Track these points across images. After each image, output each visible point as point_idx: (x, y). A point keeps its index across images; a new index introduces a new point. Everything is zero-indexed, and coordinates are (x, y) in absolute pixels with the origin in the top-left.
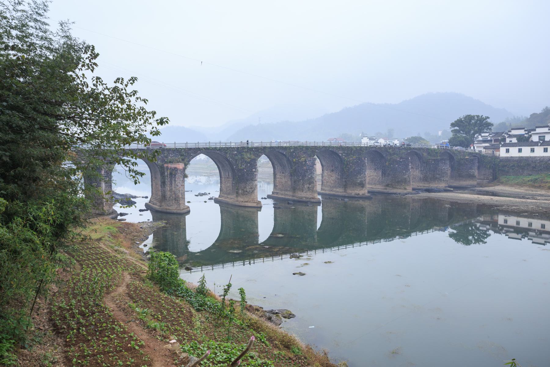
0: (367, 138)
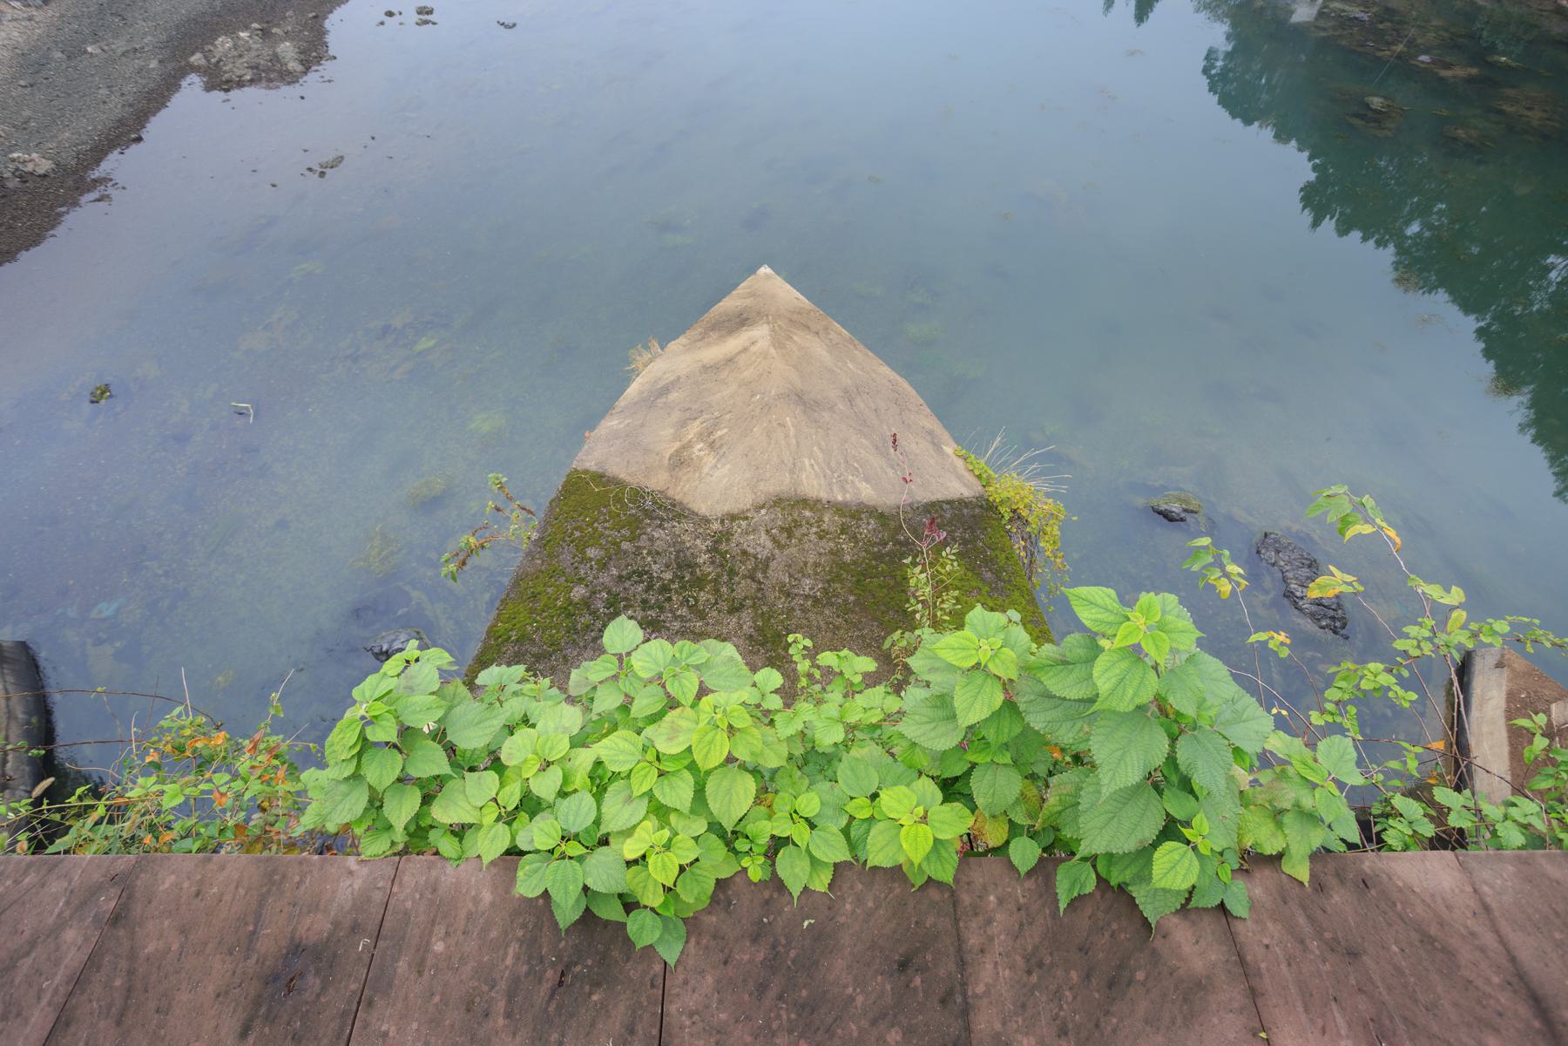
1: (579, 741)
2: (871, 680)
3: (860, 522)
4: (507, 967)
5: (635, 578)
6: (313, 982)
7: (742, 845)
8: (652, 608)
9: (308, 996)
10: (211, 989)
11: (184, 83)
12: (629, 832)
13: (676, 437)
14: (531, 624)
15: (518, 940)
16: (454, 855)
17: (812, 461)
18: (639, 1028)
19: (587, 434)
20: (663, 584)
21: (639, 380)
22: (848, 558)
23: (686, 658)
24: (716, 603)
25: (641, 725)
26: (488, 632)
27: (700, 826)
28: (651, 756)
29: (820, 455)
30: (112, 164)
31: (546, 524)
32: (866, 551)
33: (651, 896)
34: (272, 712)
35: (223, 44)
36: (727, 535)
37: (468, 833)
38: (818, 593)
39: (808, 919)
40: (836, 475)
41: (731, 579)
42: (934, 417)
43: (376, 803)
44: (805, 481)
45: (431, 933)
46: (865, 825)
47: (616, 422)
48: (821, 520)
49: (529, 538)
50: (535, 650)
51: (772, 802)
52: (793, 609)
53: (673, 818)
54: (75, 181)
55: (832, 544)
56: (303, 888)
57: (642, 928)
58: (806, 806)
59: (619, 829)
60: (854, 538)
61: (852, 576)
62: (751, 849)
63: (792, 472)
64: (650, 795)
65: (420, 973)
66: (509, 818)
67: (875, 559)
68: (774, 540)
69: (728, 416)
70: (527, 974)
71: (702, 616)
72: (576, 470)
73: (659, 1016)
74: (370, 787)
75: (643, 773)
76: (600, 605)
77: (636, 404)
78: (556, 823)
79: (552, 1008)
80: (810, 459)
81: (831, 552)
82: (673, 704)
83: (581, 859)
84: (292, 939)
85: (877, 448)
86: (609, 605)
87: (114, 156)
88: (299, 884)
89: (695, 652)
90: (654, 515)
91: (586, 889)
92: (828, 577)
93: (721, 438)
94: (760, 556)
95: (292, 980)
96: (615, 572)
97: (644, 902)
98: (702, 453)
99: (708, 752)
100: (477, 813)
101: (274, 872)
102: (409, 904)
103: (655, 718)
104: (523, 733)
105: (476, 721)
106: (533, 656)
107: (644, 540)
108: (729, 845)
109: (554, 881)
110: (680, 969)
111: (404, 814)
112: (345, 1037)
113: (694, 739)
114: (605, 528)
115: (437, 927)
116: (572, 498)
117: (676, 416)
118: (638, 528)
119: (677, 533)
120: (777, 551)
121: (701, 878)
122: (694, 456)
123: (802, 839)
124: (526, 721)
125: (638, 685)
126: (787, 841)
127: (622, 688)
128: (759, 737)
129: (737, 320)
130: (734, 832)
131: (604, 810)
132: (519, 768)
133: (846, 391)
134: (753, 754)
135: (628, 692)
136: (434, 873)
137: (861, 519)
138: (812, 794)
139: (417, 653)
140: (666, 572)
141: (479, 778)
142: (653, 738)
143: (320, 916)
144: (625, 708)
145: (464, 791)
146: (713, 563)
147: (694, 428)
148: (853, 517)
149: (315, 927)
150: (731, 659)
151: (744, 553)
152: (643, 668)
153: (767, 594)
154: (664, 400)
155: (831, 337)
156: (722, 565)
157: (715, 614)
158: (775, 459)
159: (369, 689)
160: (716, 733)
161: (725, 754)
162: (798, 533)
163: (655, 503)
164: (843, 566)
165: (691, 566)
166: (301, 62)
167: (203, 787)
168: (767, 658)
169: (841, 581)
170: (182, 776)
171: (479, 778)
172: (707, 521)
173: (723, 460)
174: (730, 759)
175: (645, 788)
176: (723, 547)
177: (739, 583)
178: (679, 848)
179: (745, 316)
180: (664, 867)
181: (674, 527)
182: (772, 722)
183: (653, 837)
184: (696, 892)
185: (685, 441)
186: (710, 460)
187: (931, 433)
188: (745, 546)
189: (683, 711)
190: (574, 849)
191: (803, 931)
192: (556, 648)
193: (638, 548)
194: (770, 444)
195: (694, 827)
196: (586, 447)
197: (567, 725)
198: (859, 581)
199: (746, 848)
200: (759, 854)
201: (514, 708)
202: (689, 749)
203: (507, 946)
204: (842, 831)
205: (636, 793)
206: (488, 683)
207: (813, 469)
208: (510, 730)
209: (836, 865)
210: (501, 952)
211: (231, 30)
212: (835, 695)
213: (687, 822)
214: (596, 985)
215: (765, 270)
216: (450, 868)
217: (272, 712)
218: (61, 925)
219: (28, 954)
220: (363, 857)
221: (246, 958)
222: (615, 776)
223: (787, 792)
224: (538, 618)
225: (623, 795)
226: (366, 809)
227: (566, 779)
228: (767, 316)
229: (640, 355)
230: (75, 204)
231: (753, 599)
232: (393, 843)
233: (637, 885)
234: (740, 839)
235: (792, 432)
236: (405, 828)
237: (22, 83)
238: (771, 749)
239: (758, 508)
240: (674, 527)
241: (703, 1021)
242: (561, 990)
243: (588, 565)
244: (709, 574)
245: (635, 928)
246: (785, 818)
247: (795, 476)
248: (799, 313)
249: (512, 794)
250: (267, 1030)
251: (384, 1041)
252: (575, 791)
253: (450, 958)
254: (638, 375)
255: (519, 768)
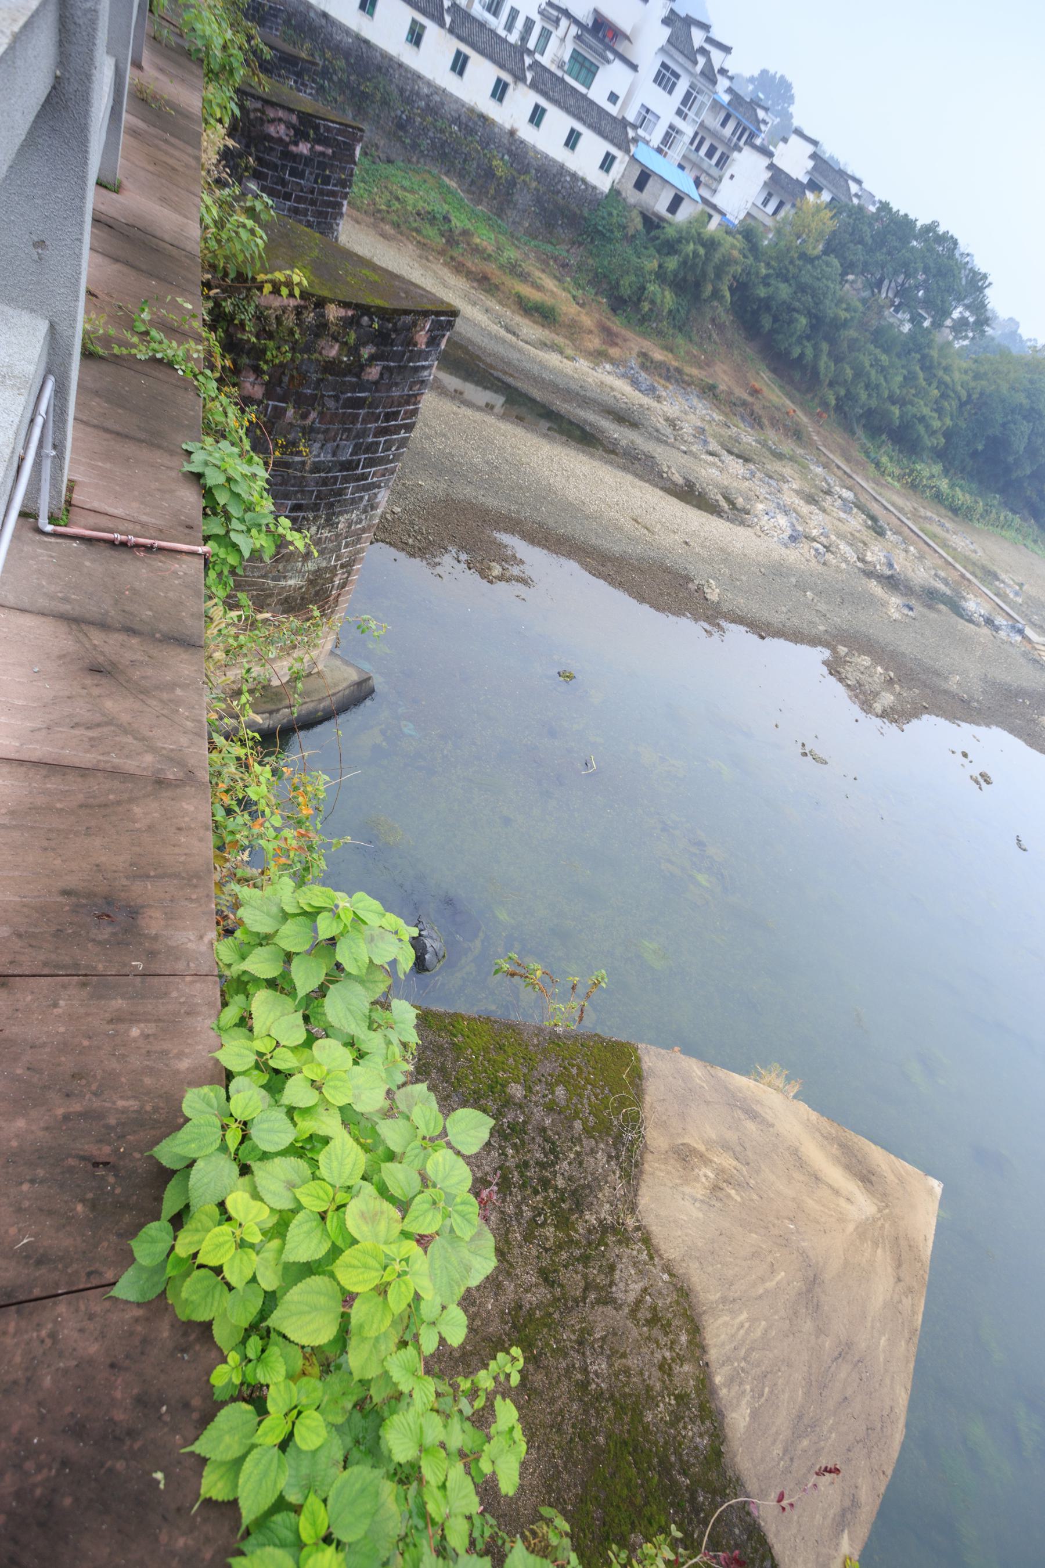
0: (810, 149)
1: (349, 1116)
2: (487, 1490)
3: (698, 1422)
4: (114, 1103)
5: (547, 1146)
6: (105, 932)
7: (254, 1343)
8: (522, 1175)
9: (94, 932)
10: (103, 859)
11: (819, 648)
12: (256, 1196)
13: (708, 1142)
14: (473, 1052)
15: (142, 1107)
16: (222, 1024)
17: (747, 1325)
18: (43, 1270)
19: (676, 1049)
20: (549, 1181)
21: (751, 1083)
22: (649, 1417)
23: (457, 1211)
24: (546, 1250)
25: (375, 1178)
26: (455, 1014)
27: (269, 1282)
28: (342, 1196)
29: (759, 1333)
30: (736, 632)
31: (575, 1037)
32: (666, 1443)
33: (187, 1241)
34: (334, 841)
35: (866, 661)
36: (625, 1240)
37: (245, 1031)
38: (594, 1386)
39: (166, 1477)
40: (743, 1364)
41: (578, 1260)
42: (878, 1501)
43: (264, 940)
44: (720, 1321)
45: (148, 1021)
46: (289, 1536)
47: (699, 1074)
48: (681, 1359)
49: (555, 1025)
50: (449, 1064)
51: (310, 1375)
52: (566, 1355)
53: (275, 1243)
54: (712, 615)
55: (658, 1386)
56: (186, 903)
57: (153, 1241)
58: (308, 1428)
59: (258, 1184)
60: (676, 1418)
61: (629, 1431)
62: (250, 1361)
63: (724, 1300)
64: (298, 1208)
65: (111, 1021)
66: (261, 1064)
67: (661, 1462)
68: (639, 1302)
69: (755, 1197)
70: (108, 1127)
71: (528, 1237)
72: (637, 1049)
73: (54, 1292)
74: (277, 931)
75: (322, 1194)
76: (510, 1117)
77: (726, 1088)
78: (259, 1110)
79: (71, 1162)
80: (748, 1319)
81: (649, 1389)
82: (403, 1207)
83: (223, 1148)
84: (143, 907)
85: (800, 1417)
86: (512, 1127)
87: (742, 629)
88: (190, 900)
89: (468, 1221)
90: (620, 1146)
91: (191, 1165)
92: (617, 1395)
93: (729, 1196)
94: (614, 1289)
95: (108, 916)
96: (548, 1122)
97: (182, 1235)
98: (703, 1179)
99: (354, 1267)
100: (264, 1032)
101: (199, 878)
102: (175, 994)
103: (383, 1192)
104: (347, 1055)
105: (352, 1008)
106: (443, 1064)
107: (588, 1143)
108: (252, 1329)
109: (198, 1126)
110: (107, 1304)
111: (256, 966)
112: (57, 972)
113: (365, 1244)
114: (589, 1098)
115: (153, 1025)
116: (608, 1055)
117: (732, 1136)
118: (600, 1132)
119: (609, 1179)
120: (627, 1310)
121: (209, 1300)
122: (697, 1170)
123: (265, 1434)
124: (360, 1056)
125: (417, 1164)
126: (262, 1411)
127: (409, 1149)
128: (383, 1330)
129: (865, 1172)
130: (268, 1330)
131: (277, 1160)
132: (312, 1060)
133: (849, 1345)
134: (361, 1326)
135: (407, 1155)
136: (204, 1009)
137: (703, 1423)
138: (324, 1432)
139: (406, 938)
140: (564, 1179)
141: (298, 1026)
142: (361, 1195)
143: (163, 922)
144: (391, 1156)
145: (283, 1015)
146: (589, 1231)
147: (726, 1161)
148: (702, 1407)
149: (153, 923)
150: (468, 1269)
151: (612, 1268)
152: (436, 1164)
153: (574, 1313)
154: (742, 1117)
155: (904, 1300)
156: (590, 1244)
157: (534, 1252)
158: (731, 1272)
159: (367, 905)
160: (377, 1270)
161: (354, 1289)
162: (656, 1332)
163: (632, 1142)
164: (638, 1415)
165: (579, 1207)
166: (884, 711)
167: (267, 811)
168: (500, 1338)
169: (618, 1417)
170: (274, 796)
171: (298, 1026)
172: (633, 1209)
173: (705, 1207)
174: (349, 1299)
175: (304, 1201)
176: (611, 1239)
177: (577, 1273)
178: (241, 1260)
179: (873, 1178)
180: (219, 1246)
181: (614, 1173)
182: (403, 1344)
183: (252, 1223)
184: (194, 1297)
185: (709, 1155)
186: (699, 1191)
187: (855, 1503)
188: (619, 1266)
189: (397, 1221)
190: (233, 1138)
191: (150, 1473)
192: (456, 1084)
193: (580, 1140)
194: (745, 1259)
195: (268, 1273)
196: (663, 1052)
197: (363, 1097)
198: (625, 1443)
199: (251, 1354)
200: (244, 1375)
201: (372, 1041)
202: (355, 1242)
203: (135, 1098)
204: (281, 1498)
205: (298, 1192)
206: (395, 1012)
207: (738, 1329)
208: (350, 1043)
209: (234, 1504)
210: (129, 1093)
211: (877, 660)
212: (458, 1436)
213: (273, 1263)
214: (93, 1206)
215: (937, 1186)
216: (211, 1022)
217: (334, 841)
218: (153, 750)
219: (136, 738)
220: (216, 943)
221: (127, 878)
222: (314, 1163)
223: (324, 1393)
224: (481, 1058)
225: (294, 1177)
226: (258, 934)
227: (306, 1111)
228: (887, 1206)
229: (778, 1076)
230: (696, 620)
231: (564, 1294)
232: (229, 966)
233: (200, 1221)
234: (260, 1342)
235: (770, 1285)
236: (245, 972)
237: (763, 570)
238: (371, 1352)
239: (668, 1269)
240: (614, 1173)
241: (44, 1353)
242: (90, 1166)
243: (547, 1092)
244: (576, 1231)
245: (153, 1233)
246: (291, 1399)
247: (721, 1306)
248: (910, 1246)
249: (285, 1061)
250: (67, 908)
251: (49, 1006)
252: (295, 1125)
253: (124, 1045)
254: (756, 1080)
255: (312, 1060)
